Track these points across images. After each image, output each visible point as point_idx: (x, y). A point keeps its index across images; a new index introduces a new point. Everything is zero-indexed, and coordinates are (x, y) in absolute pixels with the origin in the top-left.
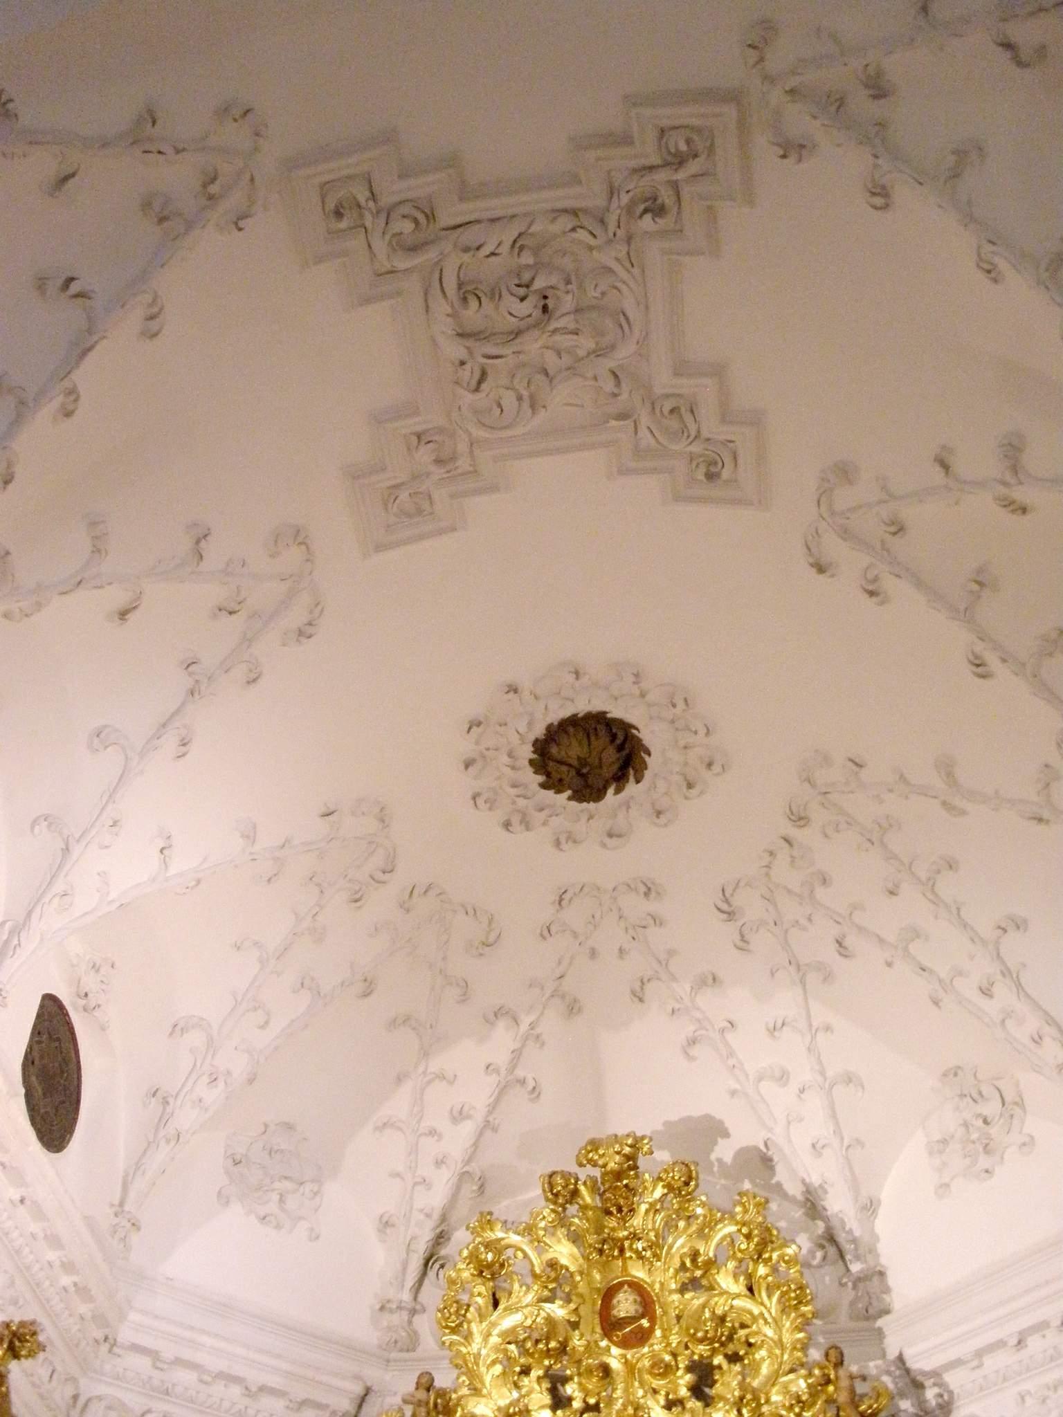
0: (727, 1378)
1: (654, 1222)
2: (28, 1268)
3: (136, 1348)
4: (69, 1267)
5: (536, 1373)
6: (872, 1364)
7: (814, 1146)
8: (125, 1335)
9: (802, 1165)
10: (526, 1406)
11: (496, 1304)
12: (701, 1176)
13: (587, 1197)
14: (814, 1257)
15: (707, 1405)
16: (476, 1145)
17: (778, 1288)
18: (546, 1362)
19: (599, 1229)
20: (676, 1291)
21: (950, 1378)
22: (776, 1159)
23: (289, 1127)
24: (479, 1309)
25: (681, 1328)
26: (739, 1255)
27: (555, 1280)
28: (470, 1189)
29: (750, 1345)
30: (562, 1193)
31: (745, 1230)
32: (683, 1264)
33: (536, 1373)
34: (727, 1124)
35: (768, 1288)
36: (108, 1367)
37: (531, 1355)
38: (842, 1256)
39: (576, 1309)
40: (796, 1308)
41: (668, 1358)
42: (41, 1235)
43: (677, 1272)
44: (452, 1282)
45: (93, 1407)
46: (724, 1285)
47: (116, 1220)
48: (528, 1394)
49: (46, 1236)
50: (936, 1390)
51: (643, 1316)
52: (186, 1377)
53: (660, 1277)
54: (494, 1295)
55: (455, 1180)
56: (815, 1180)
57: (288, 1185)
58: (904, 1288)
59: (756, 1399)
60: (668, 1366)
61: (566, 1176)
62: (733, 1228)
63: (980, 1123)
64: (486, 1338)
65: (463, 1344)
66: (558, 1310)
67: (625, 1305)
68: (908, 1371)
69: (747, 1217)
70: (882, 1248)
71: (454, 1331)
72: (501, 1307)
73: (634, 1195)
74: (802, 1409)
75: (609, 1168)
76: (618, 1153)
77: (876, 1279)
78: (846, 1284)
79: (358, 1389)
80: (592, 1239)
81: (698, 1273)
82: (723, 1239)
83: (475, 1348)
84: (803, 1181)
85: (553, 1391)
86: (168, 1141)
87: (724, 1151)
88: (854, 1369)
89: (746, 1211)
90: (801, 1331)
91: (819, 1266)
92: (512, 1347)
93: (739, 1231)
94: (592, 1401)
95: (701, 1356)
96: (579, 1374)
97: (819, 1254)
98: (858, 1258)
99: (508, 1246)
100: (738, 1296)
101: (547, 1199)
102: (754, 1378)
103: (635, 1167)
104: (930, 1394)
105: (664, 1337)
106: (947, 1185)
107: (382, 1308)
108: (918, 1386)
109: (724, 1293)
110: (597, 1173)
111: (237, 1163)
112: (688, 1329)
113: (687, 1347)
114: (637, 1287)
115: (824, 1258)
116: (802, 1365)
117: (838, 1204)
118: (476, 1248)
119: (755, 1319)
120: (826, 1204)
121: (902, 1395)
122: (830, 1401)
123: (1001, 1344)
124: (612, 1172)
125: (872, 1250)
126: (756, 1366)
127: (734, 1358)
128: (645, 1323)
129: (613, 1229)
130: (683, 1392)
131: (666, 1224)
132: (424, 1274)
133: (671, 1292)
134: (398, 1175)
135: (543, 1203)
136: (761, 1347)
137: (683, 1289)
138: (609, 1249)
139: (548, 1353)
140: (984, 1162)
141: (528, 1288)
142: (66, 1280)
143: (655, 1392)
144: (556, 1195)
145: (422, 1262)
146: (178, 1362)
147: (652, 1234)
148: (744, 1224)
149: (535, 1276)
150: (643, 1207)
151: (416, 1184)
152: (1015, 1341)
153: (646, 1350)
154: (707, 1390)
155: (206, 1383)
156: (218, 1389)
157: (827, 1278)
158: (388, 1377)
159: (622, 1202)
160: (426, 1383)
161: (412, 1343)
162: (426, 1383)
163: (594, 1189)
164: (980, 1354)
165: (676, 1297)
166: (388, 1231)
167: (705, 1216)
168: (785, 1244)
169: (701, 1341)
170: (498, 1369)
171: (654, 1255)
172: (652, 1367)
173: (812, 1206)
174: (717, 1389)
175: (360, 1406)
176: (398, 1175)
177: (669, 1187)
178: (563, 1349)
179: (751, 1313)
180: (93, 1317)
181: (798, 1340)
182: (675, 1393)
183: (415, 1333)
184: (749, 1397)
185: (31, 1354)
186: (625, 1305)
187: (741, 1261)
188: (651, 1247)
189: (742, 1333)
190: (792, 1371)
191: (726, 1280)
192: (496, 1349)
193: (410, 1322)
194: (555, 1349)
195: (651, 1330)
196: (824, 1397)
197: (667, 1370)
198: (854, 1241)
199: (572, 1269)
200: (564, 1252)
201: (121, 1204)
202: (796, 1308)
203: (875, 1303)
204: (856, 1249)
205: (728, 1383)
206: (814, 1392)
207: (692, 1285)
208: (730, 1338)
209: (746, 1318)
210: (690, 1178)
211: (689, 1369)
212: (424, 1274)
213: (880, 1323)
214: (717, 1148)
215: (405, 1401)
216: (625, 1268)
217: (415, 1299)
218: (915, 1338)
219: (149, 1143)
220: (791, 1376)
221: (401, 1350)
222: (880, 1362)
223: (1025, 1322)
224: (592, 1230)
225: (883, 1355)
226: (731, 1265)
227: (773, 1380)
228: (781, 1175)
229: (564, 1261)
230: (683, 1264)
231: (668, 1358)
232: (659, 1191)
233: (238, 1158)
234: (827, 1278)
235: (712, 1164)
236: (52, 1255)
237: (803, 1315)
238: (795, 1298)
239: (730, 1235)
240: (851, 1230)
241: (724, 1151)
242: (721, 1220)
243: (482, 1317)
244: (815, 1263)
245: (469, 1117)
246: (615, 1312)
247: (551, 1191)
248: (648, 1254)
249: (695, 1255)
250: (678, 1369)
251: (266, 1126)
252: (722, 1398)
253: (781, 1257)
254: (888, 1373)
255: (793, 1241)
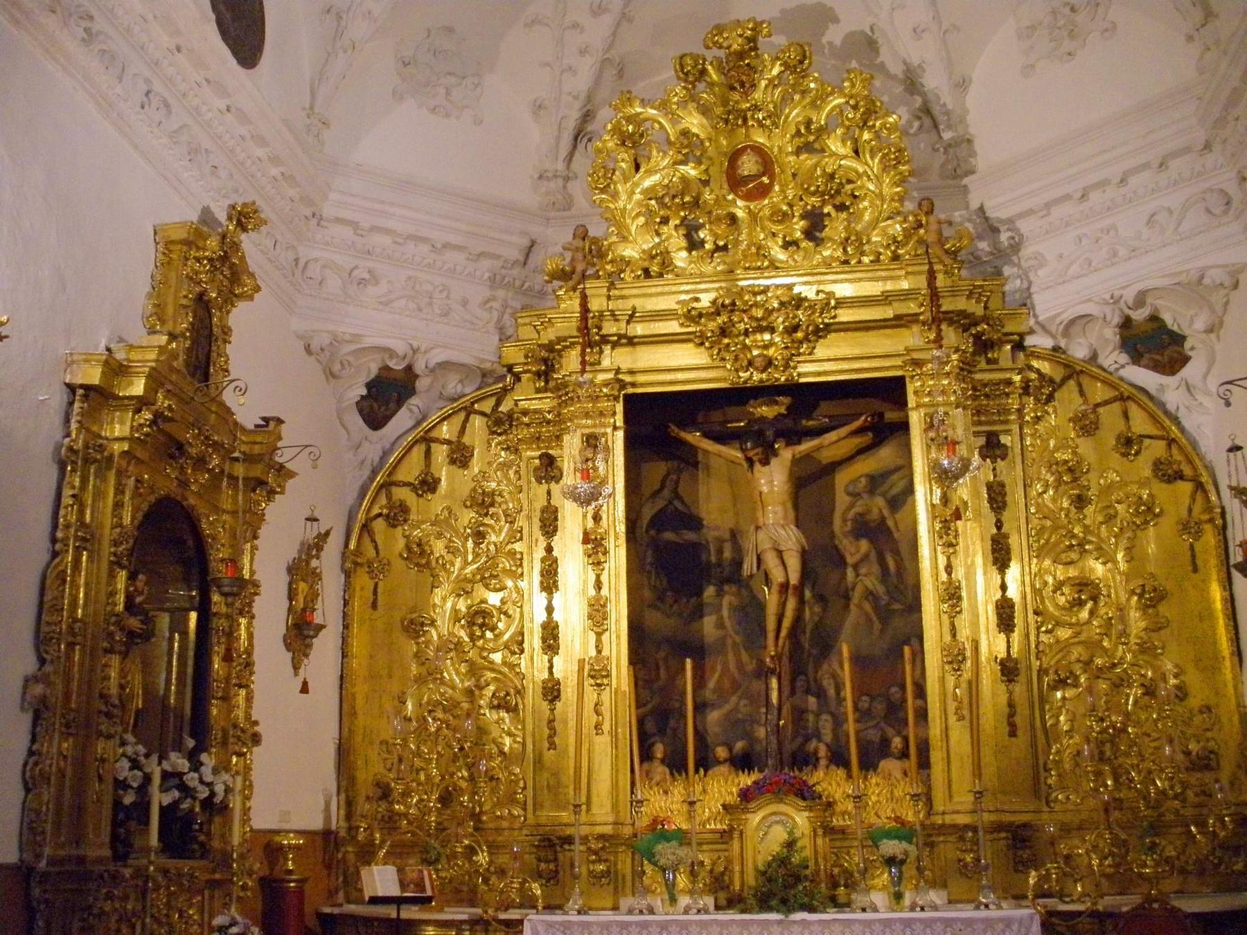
0: (835, 224)
1: (773, 95)
2: (242, 164)
3: (339, 220)
4: (275, 160)
5: (674, 222)
6: (957, 214)
7: (915, 31)
8: (328, 211)
9: (904, 45)
10: (666, 248)
11: (637, 168)
12: (814, 58)
13: (714, 75)
14: (911, 127)
15: (817, 245)
16: (614, 34)
17: (880, 150)
18: (682, 214)
19: (725, 102)
20: (792, 153)
21: (1024, 226)
22: (880, 41)
23: (450, 30)
24: (623, 174)
25: (796, 184)
26: (847, 123)
27: (688, 147)
28: (610, 73)
29: (855, 197)
30: (691, 73)
31: (852, 102)
32: (798, 131)
33: (674, 222)
34: (837, 11)
35: (871, 150)
36: (318, 237)
37: (669, 208)
38: (936, 126)
39: (706, 170)
40: (895, 167)
41: (785, 208)
42: (248, 137)
43: (793, 137)
44: (599, 151)
45: (311, 266)
46: (833, 148)
47: (309, 122)
48: (667, 239)
49: (252, 137)
50: (1009, 234)
51: (764, 174)
52: (385, 240)
53: (778, 142)
54: (635, 160)
55: (598, 65)
56: (915, 61)
57: (453, 80)
58: (987, 154)
59: (859, 239)
60: (785, 214)
61: (695, 58)
62: (842, 100)
63: (1067, 10)
64: (631, 195)
65: (609, 201)
66: (691, 171)
67: (748, 165)
68: (987, 219)
69: (854, 91)
70: (970, 118)
71: (603, 191)
72: (642, 170)
73: (755, 72)
74: (897, 247)
75: (732, 49)
76: (741, 36)
77: (964, 145)
78: (938, 150)
79: (525, 242)
80: (719, 110)
81: (812, 138)
82: (832, 109)
83: (621, 204)
84: (905, 63)
85: (688, 236)
86: (345, 51)
87: (834, 35)
88: (942, 216)
89: (853, 85)
90: (898, 186)
91: (915, 135)
92: (653, 202)
93: (847, 102)
94: (721, 243)
95: (814, 206)
96: (711, 223)
97: (916, 124)
98: (949, 127)
99: (646, 120)
100: (845, 157)
101: (679, 78)
102: (857, 223)
103: (755, 49)
104: (1004, 237)
105: (783, 191)
106: (1033, 66)
107: (540, 177)
108: (995, 231)
109: (833, 154)
110: (722, 54)
111: (406, 65)
112: (802, 185)
113: (801, 199)
114: (758, 150)
115: (921, 127)
116: (899, 213)
117: (933, 81)
118: (619, 122)
119: (860, 176)
120: (924, 81)
121: (980, 237)
122: (921, 242)
123: (1067, 197)
124: (735, 52)
125: (962, 120)
126: (858, 216)
127: (841, 208)
128: (765, 180)
129: (737, 102)
130: (798, 234)
131: (783, 99)
132: (575, 147)
133: (788, 154)
134: (548, 64)
135: (675, 81)
136: (864, 199)
137: (798, 152)
138: (735, 119)
139: (683, 206)
140: (1067, 45)
141: (665, 153)
142: (275, 171)
143: (774, 235)
144: (686, 74)
145: (571, 137)
146: (375, 229)
147: (771, 106)
148: (851, 97)
149: (669, 143)
150: (763, 83)
151: (562, 72)
152: (1079, 195)
153: (766, 201)
154: (818, 234)
155: (399, 244)
156: (410, 247)
157: (922, 145)
158: (550, 231)
159: (744, 78)
160: (582, 233)
161: (568, 204)
162: (582, 233)
163: (720, 69)
164: (1048, 206)
165: (792, 158)
166: (542, 113)
167: (817, 90)
168: (888, 114)
169: (813, 194)
170: (642, 220)
171: (774, 123)
172: (772, 215)
173: (912, 83)
174: (827, 232)
175: (527, 255)
176: (548, 64)
177: (786, 65)
178: (696, 203)
179: (857, 172)
180: (301, 198)
181: (897, 193)
182: (791, 235)
183: (570, 196)
184: (853, 238)
185: (256, 228)
186: (748, 165)
187: (848, 128)
188: (769, 117)
189: (849, 187)
190: (889, 218)
191: (835, 144)
192: (639, 204)
193: (565, 187)
194: (689, 203)
195: (771, 185)
196: (916, 238)
197: (784, 218)
198: (947, 113)
199: (702, 136)
200: (694, 122)
201: (312, 108)
202: (895, 167)
203: (962, 165)
204: (949, 119)
205: (836, 227)
206: (908, 234)
207: (807, 148)
208: (838, 192)
209: (852, 176)
210: (804, 57)
211: (802, 217)
212: (575, 147)
213: (965, 181)
214: (828, 32)
215: (565, 249)
216: (747, 136)
217: (568, 168)
218: (994, 194)
219: (329, 54)
220: (889, 222)
221: (559, 210)
222: (964, 212)
223: (1093, 178)
224: (719, 103)
225: (967, 208)
226: (839, 131)
227: (874, 224)
228: (885, 56)
229: (695, 130)
230: (798, 131)
231: (785, 208)
232: (776, 70)
233: (407, 61)
234: (922, 145)
235: (823, 47)
236: (260, 152)
237: (901, 173)
238: (893, 160)
239: (839, 106)
240: (945, 105)
241: (834, 35)
242: (832, 93)
243: (626, 179)
244: (912, 131)
245: (606, 10)
246: (739, 171)
247: (682, 70)
248: (768, 122)
249: (808, 123)
250: (793, 216)
251: (429, 31)
252: (830, 239)
253: (884, 125)
254: (969, 220)
255: (894, 113)
